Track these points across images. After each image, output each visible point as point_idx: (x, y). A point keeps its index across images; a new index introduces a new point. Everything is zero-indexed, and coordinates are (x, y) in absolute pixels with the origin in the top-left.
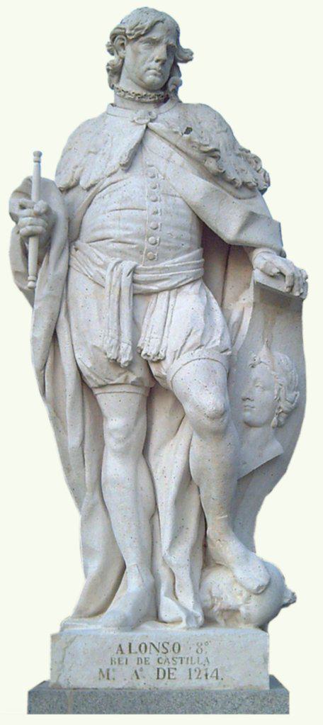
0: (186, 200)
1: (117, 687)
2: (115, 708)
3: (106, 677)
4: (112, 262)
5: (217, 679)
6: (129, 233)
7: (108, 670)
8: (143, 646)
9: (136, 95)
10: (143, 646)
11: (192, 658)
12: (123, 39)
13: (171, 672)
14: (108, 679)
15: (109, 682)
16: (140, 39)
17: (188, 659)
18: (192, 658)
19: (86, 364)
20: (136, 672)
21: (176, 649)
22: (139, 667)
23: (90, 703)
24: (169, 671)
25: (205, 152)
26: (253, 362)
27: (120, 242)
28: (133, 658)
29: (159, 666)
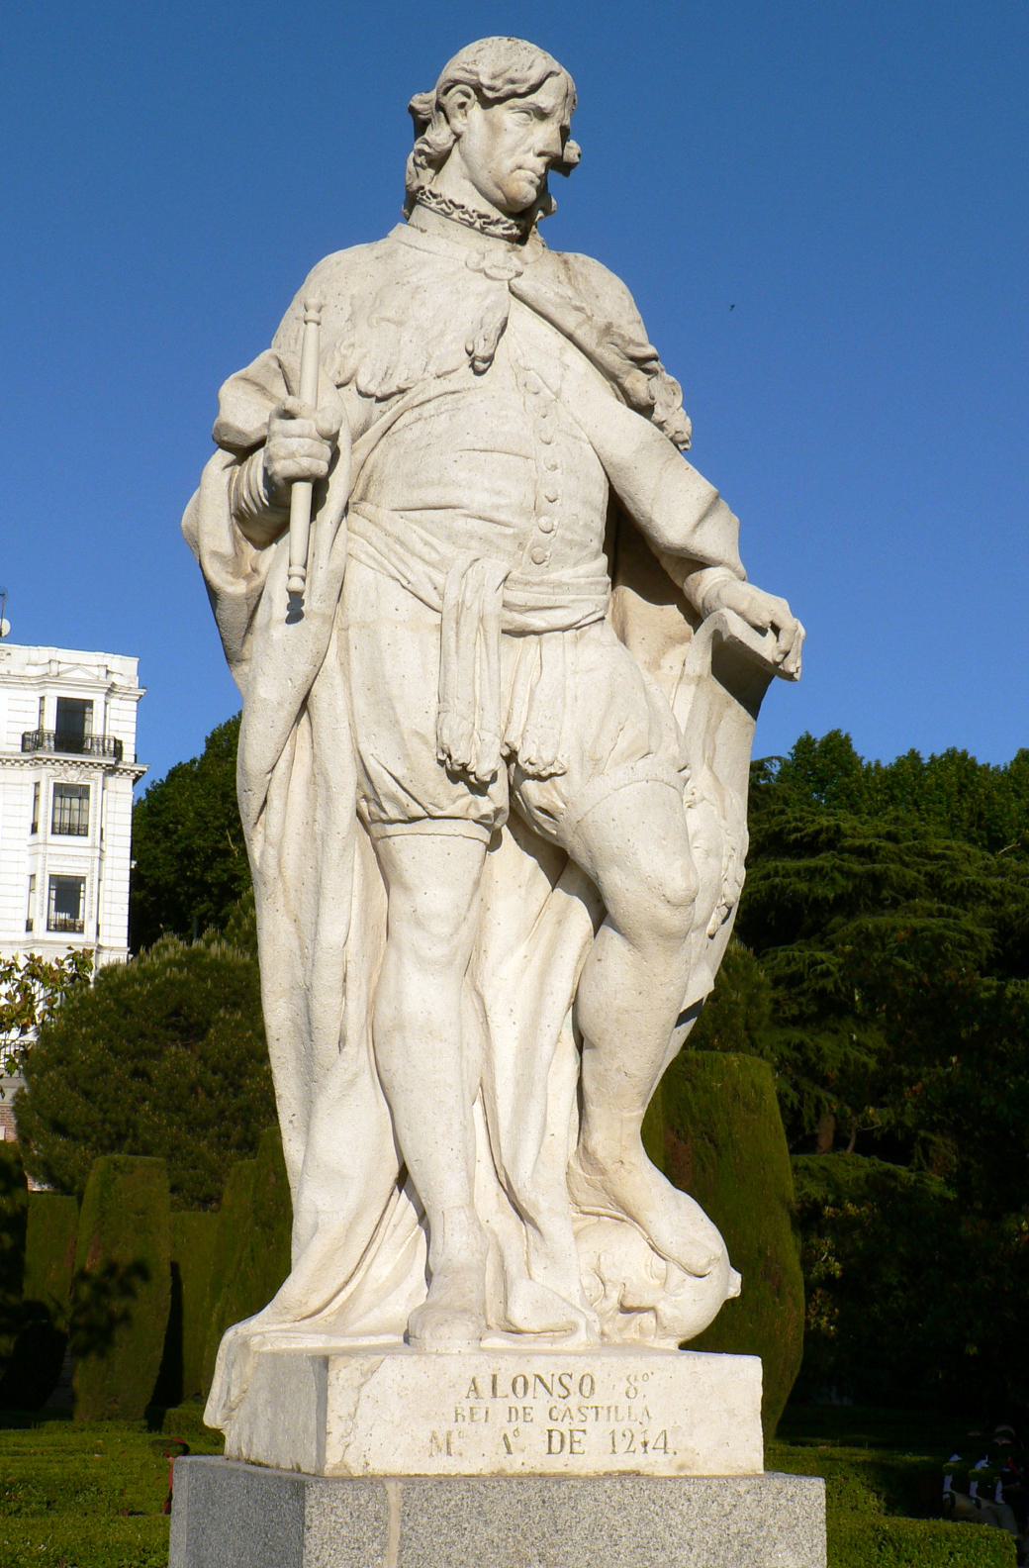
0: (601, 451)
1: (466, 1473)
2: (489, 1517)
3: (444, 1448)
4: (462, 561)
5: (665, 1452)
6: (503, 501)
7: (449, 1434)
8: (520, 1381)
9: (480, 216)
10: (520, 1381)
11: (616, 1407)
12: (468, 96)
13: (576, 1439)
14: (449, 1454)
15: (451, 1460)
16: (510, 102)
17: (609, 1408)
18: (616, 1407)
19: (384, 760)
20: (505, 1437)
21: (586, 1388)
22: (513, 1426)
23: (436, 1507)
24: (572, 1436)
25: (632, 359)
26: (690, 797)
27: (480, 518)
28: (500, 1407)
29: (552, 1425)
